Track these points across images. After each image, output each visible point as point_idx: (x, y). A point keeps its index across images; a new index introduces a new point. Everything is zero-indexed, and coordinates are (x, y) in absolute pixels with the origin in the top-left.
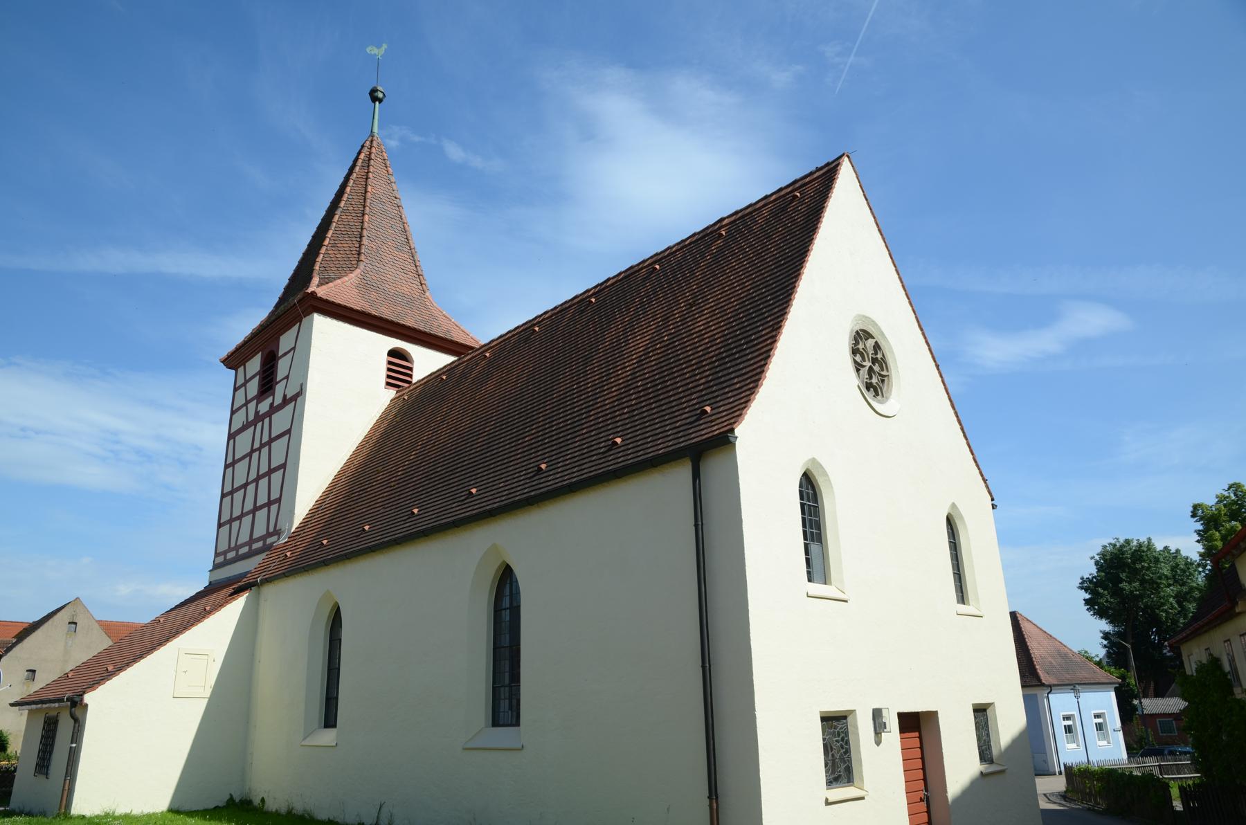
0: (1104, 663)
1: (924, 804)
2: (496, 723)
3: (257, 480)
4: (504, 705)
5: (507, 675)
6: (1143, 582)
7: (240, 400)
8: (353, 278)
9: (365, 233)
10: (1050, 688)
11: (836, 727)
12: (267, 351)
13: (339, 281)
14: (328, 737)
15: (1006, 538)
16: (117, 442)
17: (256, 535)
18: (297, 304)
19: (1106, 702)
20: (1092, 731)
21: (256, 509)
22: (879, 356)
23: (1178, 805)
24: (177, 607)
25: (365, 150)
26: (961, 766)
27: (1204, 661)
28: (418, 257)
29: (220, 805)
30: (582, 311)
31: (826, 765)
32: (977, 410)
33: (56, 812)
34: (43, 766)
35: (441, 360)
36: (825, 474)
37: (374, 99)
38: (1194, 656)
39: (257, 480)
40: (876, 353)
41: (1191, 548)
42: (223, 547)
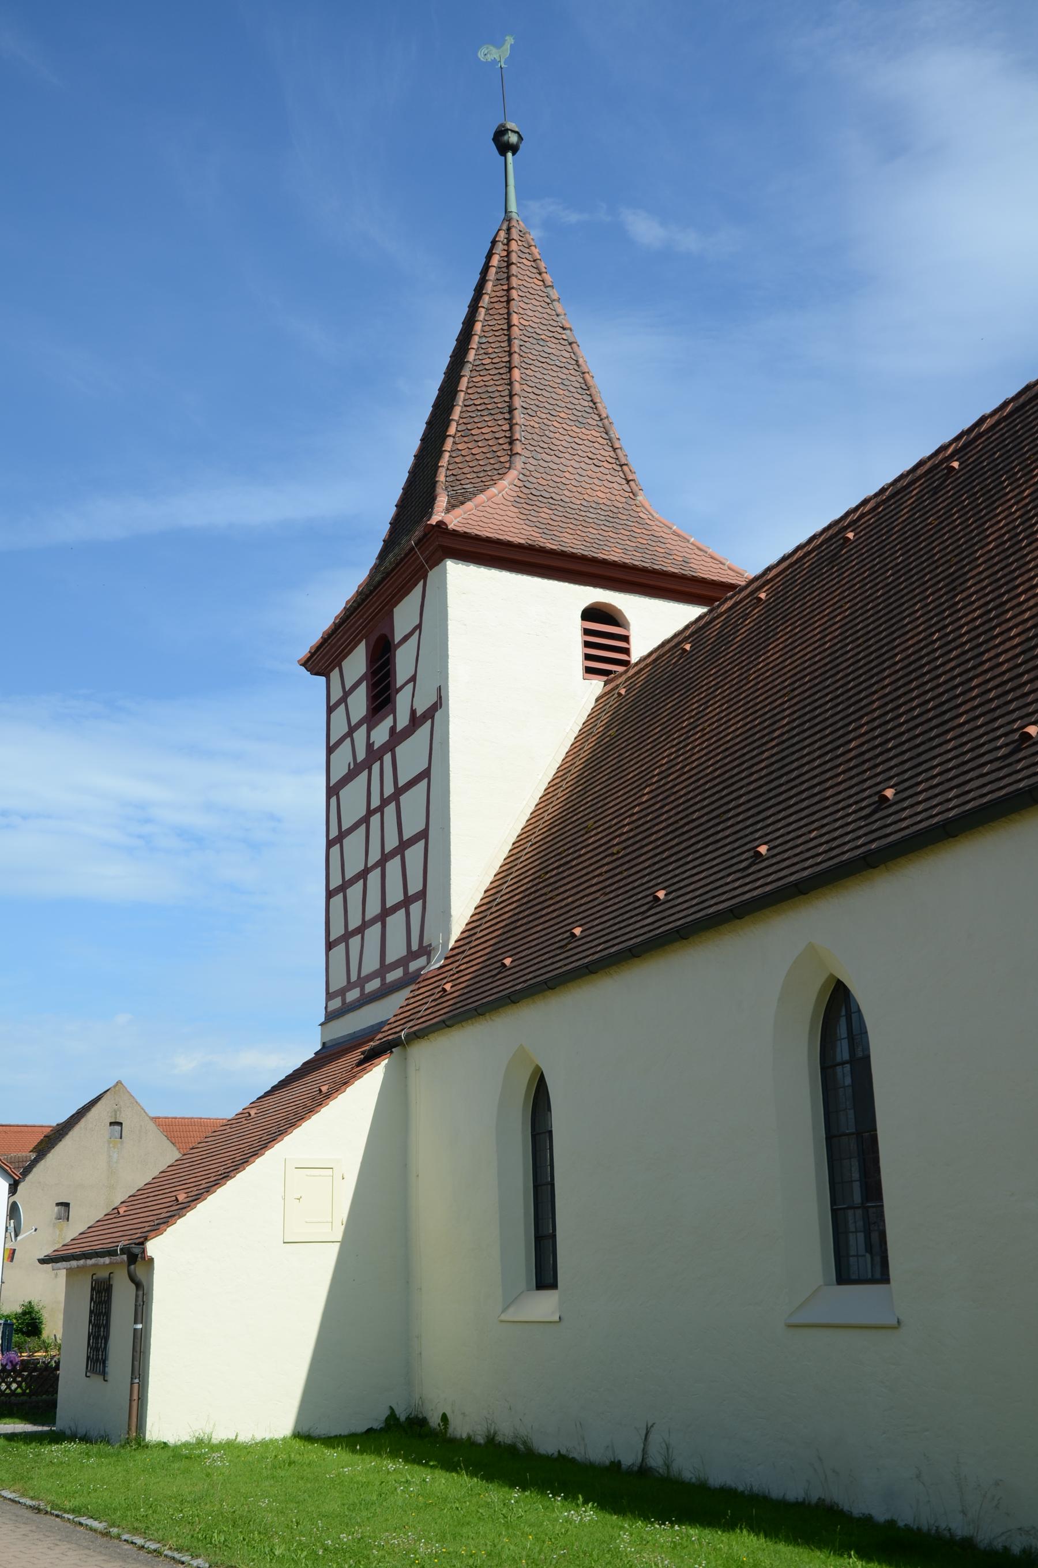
2: (843, 1277)
3: (382, 863)
4: (857, 1242)
5: (857, 1187)
7: (340, 728)
8: (505, 487)
9: (517, 402)
12: (374, 637)
13: (482, 497)
14: (544, 1306)
16: (148, 821)
17: (390, 959)
18: (416, 548)
21: (386, 912)
24: (275, 1089)
25: (500, 248)
28: (616, 432)
29: (377, 1425)
30: (936, 490)
33: (124, 1436)
34: (97, 1360)
35: (679, 615)
37: (504, 147)
39: (382, 863)
42: (339, 982)
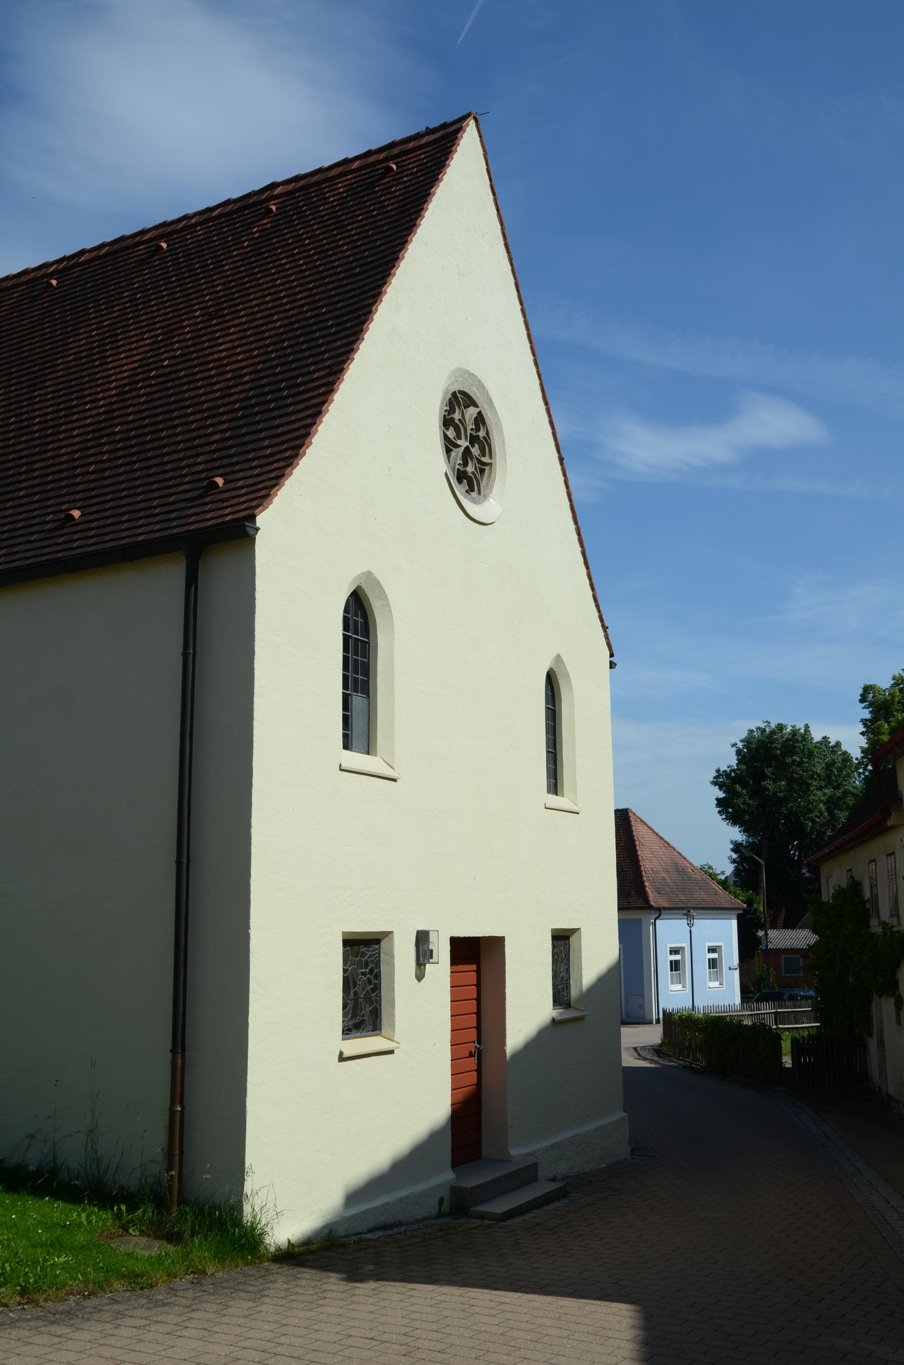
0: (731, 882)
1: (474, 1060)
6: (790, 781)
10: (659, 912)
11: (363, 957)
15: (623, 708)
19: (723, 933)
20: (702, 969)
22: (482, 434)
23: (787, 1061)
26: (527, 1007)
27: (844, 886)
31: (345, 1006)
32: (613, 531)
36: (383, 596)
38: (833, 879)
40: (477, 429)
41: (852, 741)
